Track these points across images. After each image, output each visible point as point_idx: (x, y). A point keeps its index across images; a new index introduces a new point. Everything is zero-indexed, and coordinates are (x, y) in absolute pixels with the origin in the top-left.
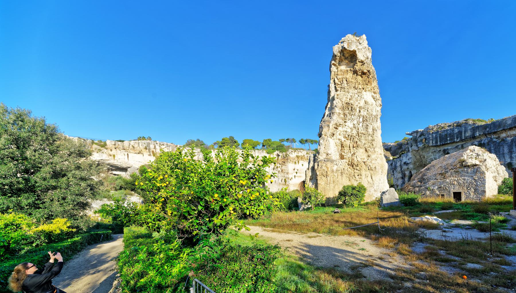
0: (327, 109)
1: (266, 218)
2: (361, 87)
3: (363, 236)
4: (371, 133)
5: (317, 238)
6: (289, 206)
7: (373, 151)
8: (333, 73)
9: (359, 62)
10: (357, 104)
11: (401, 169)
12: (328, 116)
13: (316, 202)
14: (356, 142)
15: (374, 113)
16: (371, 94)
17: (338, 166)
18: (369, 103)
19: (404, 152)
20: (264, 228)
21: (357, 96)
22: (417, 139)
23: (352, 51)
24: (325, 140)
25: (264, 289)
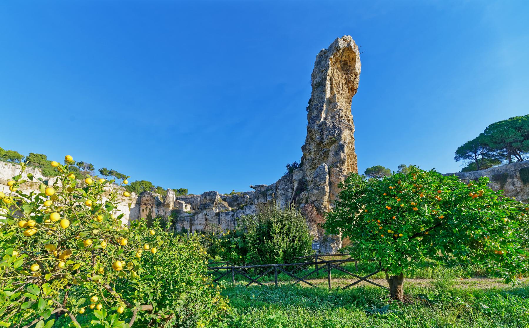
25: (94, 268)
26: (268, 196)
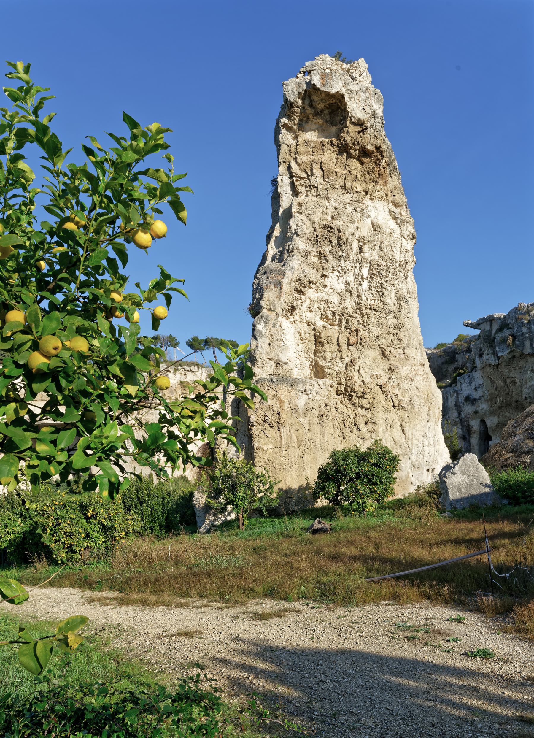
0: (273, 240)
1: (94, 560)
2: (359, 189)
3: (446, 602)
4: (393, 308)
5: (290, 618)
6: (167, 519)
7: (402, 356)
8: (284, 149)
9: (353, 123)
10: (351, 230)
11: (460, 414)
12: (276, 261)
13: (250, 503)
14: (357, 331)
15: (398, 257)
16: (386, 207)
17: (311, 396)
18: (384, 228)
19: (462, 371)
20: (88, 593)
21: (350, 209)
22: (494, 338)
23: (333, 96)
24: (271, 324)
26: (499, 345)
